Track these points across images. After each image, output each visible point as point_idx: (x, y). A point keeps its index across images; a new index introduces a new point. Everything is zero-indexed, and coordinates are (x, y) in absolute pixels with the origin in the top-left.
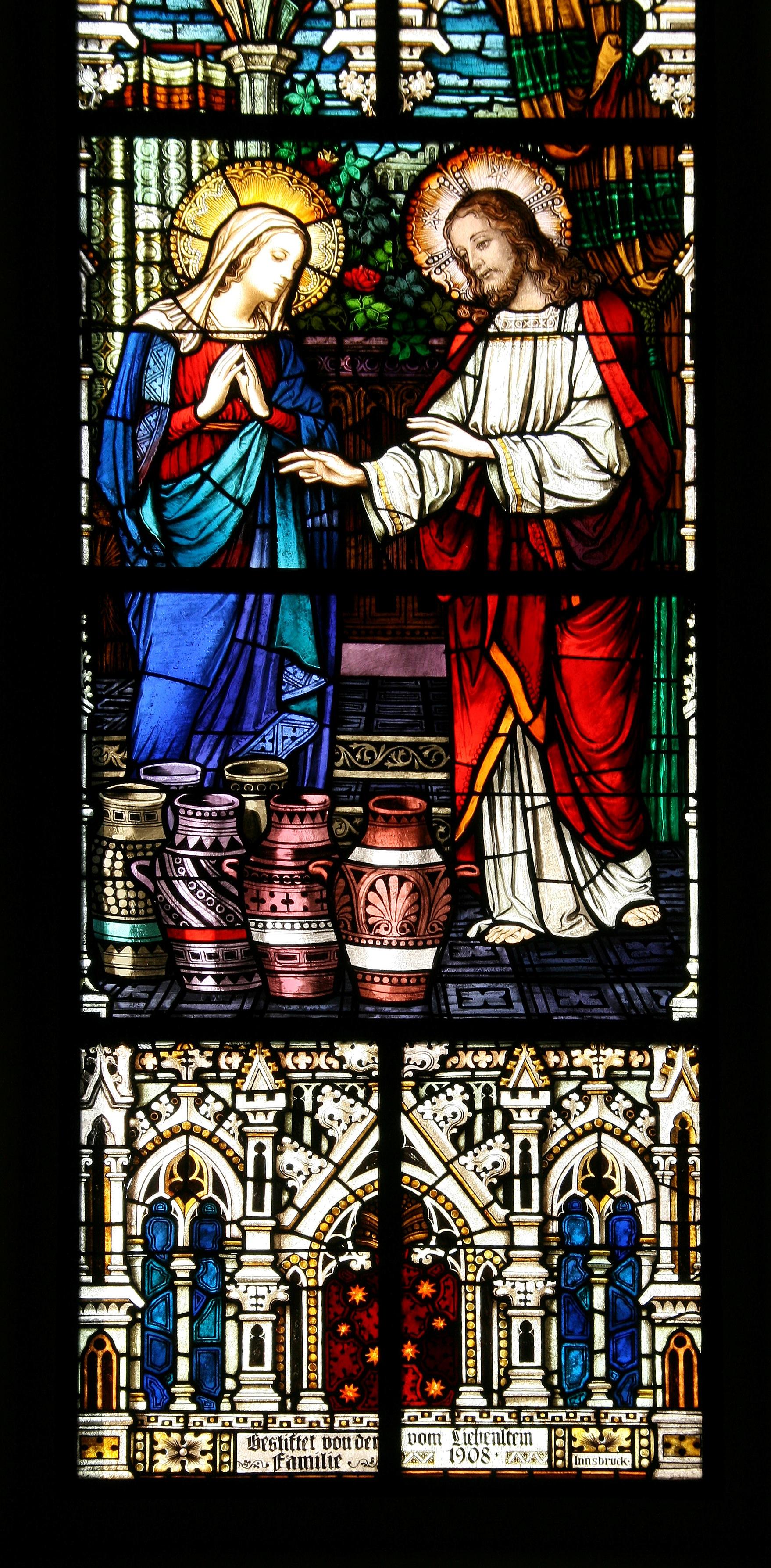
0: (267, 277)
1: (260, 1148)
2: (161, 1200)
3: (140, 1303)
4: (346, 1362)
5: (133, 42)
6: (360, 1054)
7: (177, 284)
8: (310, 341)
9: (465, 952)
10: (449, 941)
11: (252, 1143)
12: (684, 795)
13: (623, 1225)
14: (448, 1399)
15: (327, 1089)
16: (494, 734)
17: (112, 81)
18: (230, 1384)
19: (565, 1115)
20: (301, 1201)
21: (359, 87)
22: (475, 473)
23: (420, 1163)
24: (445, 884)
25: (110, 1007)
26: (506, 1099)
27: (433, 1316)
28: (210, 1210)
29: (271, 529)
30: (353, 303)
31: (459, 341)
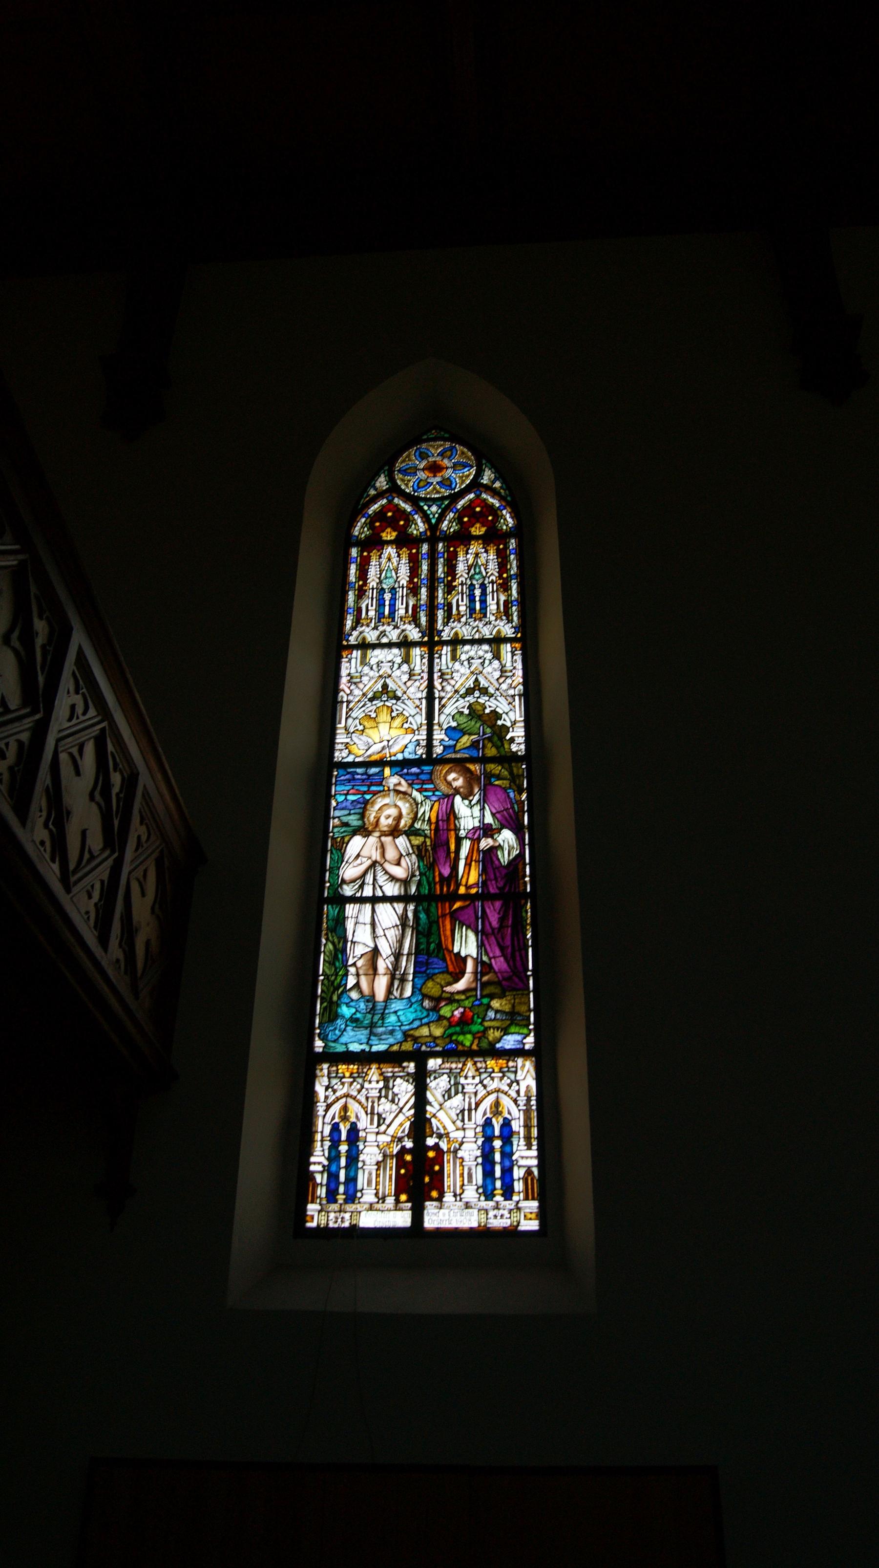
3: (326, 1163)
11: (370, 1100)
14: (440, 1199)
18: (359, 1195)
20: (387, 1122)
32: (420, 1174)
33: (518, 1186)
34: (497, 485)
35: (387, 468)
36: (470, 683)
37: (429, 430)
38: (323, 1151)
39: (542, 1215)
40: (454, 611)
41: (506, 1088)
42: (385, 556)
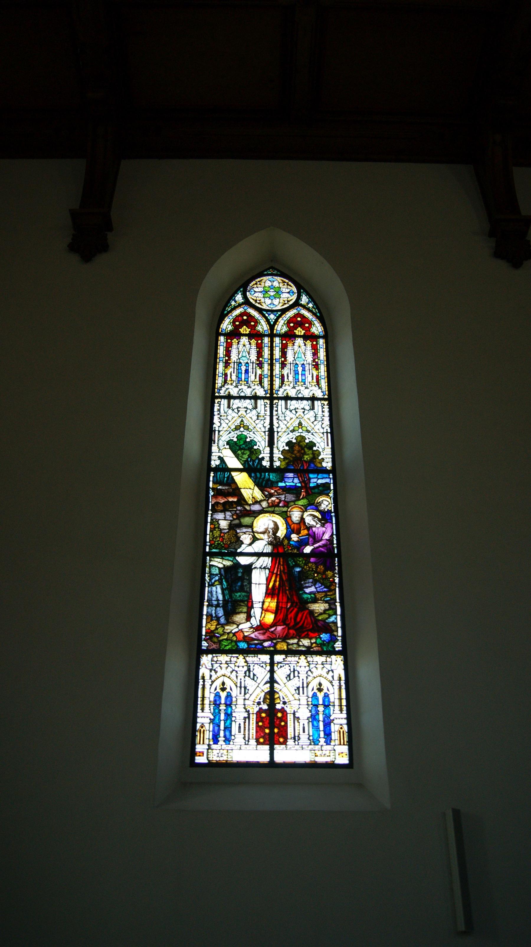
3: (212, 717)
14: (285, 743)
18: (233, 738)
20: (250, 692)
32: (272, 725)
33: (335, 736)
34: (310, 305)
35: (242, 289)
36: (238, 422)
37: (269, 269)
38: (210, 710)
42: (241, 343)
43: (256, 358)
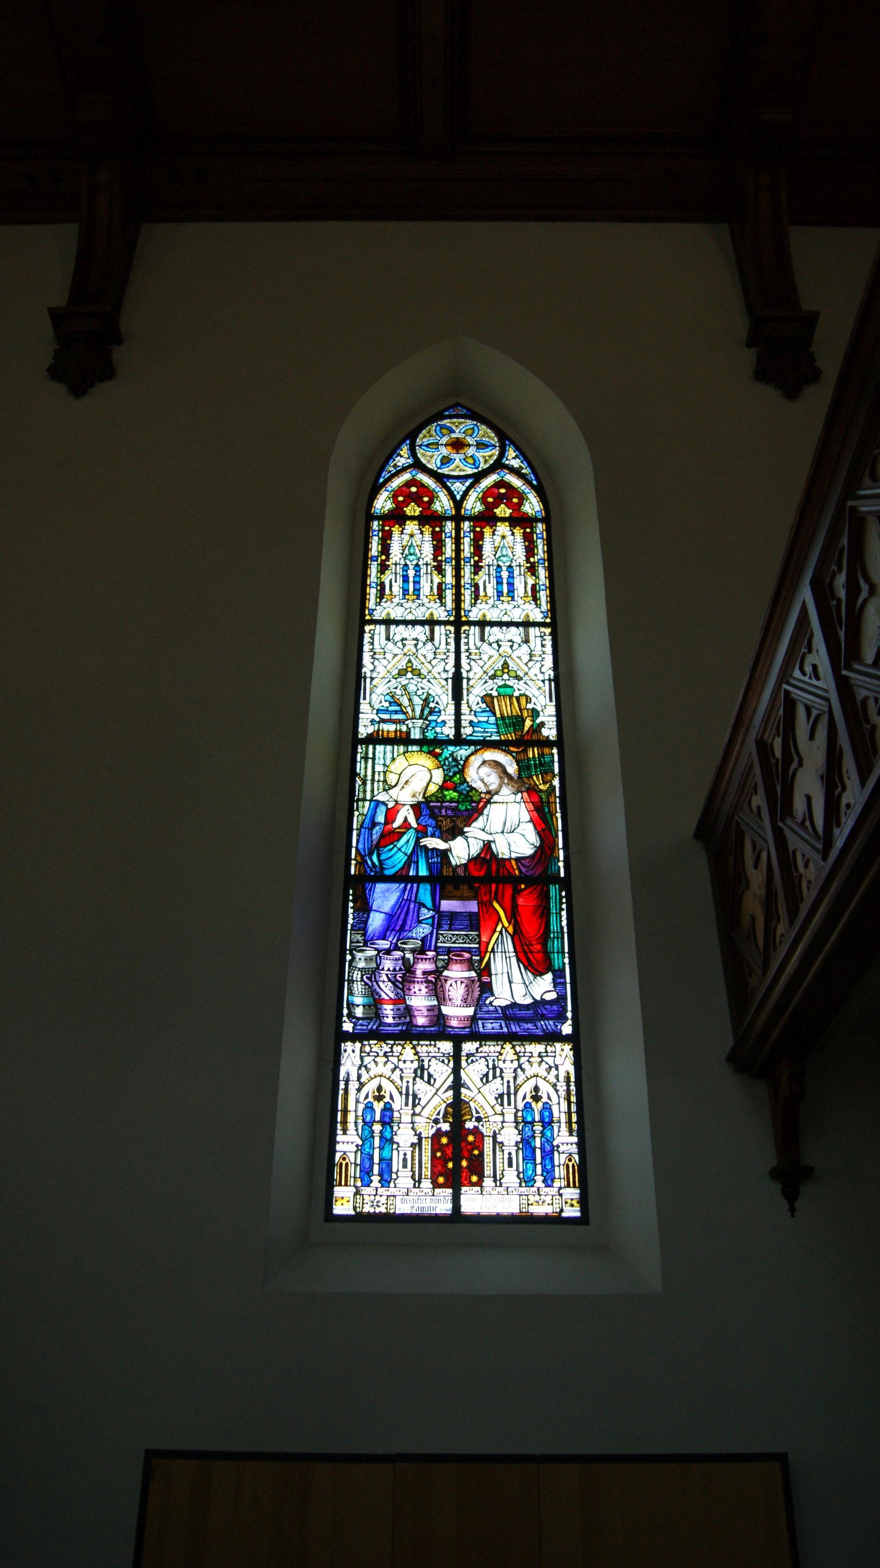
0: (417, 785)
1: (408, 1082)
2: (369, 1102)
3: (360, 1143)
4: (440, 1168)
5: (378, 719)
6: (447, 1047)
7: (388, 788)
8: (432, 804)
9: (485, 1009)
10: (479, 1004)
11: (405, 1080)
12: (563, 953)
13: (546, 1114)
14: (479, 1184)
15: (433, 1059)
16: (495, 931)
17: (370, 730)
18: (394, 1176)
19: (523, 1070)
20: (423, 1103)
21: (449, 731)
22: (487, 846)
23: (468, 1088)
24: (478, 984)
25: (353, 1028)
26: (501, 1064)
27: (473, 1150)
28: (388, 1106)
29: (417, 863)
30: (446, 793)
31: (481, 804)
32: (457, 1154)
36: (403, 664)
39: (583, 1201)
40: (482, 593)
41: (545, 1074)
43: (432, 557)
